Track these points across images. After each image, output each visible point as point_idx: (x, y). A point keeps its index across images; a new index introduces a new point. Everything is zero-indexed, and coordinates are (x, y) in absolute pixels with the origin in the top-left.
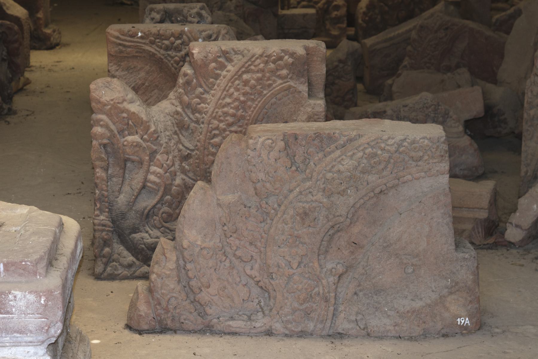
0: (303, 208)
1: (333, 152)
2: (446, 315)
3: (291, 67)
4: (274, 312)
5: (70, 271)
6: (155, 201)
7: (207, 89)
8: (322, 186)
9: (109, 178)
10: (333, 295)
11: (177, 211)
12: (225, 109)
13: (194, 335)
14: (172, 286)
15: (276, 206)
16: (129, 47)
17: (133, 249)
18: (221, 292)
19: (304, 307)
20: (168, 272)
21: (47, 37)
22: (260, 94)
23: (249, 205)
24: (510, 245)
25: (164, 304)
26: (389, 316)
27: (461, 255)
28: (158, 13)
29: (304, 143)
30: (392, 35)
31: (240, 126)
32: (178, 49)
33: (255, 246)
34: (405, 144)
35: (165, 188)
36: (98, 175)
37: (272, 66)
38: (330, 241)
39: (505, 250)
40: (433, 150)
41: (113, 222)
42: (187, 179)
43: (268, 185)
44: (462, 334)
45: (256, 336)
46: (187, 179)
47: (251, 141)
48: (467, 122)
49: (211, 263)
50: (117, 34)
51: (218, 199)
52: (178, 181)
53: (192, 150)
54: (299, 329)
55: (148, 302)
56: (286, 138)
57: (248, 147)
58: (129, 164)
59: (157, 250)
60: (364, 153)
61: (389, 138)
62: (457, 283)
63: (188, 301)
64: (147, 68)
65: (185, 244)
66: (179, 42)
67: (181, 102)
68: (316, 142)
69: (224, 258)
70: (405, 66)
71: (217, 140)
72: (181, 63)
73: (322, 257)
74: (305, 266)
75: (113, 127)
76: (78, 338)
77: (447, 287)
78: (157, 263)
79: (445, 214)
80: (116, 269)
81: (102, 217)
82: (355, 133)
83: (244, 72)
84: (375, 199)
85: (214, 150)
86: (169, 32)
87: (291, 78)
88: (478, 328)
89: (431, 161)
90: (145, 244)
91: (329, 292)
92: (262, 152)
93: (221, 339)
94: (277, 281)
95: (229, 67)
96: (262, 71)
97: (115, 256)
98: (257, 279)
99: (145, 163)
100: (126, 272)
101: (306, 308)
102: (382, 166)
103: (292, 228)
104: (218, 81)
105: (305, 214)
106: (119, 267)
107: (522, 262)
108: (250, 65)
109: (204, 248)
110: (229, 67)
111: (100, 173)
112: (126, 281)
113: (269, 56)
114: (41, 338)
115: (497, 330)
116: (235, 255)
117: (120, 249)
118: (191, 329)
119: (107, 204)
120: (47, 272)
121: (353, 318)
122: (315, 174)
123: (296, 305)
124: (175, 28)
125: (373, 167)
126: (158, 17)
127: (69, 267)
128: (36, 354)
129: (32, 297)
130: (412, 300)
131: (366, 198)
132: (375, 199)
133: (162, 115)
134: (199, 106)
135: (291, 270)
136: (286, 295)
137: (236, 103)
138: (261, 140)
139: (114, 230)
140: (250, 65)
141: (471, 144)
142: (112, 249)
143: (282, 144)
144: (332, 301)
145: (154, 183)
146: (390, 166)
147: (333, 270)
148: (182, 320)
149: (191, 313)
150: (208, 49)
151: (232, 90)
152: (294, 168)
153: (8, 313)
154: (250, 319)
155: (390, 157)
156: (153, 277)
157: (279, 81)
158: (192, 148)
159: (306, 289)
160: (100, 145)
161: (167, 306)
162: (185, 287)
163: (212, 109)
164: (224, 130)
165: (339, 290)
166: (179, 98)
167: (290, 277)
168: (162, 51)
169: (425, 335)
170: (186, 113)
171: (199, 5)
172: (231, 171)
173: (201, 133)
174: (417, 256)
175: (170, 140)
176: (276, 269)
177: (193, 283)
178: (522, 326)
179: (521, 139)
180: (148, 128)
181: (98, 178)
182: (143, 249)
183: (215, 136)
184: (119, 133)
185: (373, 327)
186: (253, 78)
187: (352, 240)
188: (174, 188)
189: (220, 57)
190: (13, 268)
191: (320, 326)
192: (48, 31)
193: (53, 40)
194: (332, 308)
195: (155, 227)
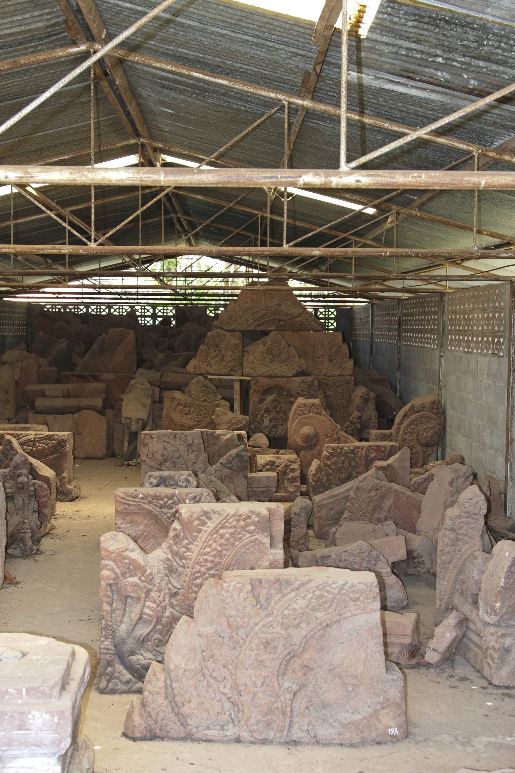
0: (266, 638)
1: (290, 593)
2: (380, 726)
3: (257, 524)
4: (242, 722)
5: (79, 694)
6: (148, 630)
7: (191, 540)
8: (281, 621)
9: (113, 611)
10: (289, 709)
11: (167, 638)
12: (206, 557)
13: (178, 742)
14: (161, 702)
15: (244, 636)
16: (132, 505)
17: (131, 668)
18: (200, 707)
19: (266, 719)
20: (158, 690)
21: (70, 492)
22: (233, 545)
23: (223, 635)
24: (428, 665)
25: (154, 716)
26: (334, 727)
27: (390, 677)
28: (155, 478)
29: (267, 586)
30: (335, 493)
31: (217, 570)
32: (170, 507)
33: (228, 668)
34: (346, 587)
35: (157, 619)
36: (104, 608)
37: (242, 523)
38: (287, 665)
39: (425, 670)
40: (368, 593)
41: (115, 646)
42: (175, 612)
43: (238, 620)
44: (392, 742)
45: (228, 743)
46: (175, 612)
47: (225, 585)
48: (393, 563)
49: (192, 682)
50: (123, 495)
51: (199, 631)
52: (167, 614)
53: (179, 589)
54: (262, 737)
55: (141, 715)
56: (252, 582)
57: (222, 589)
58: (129, 600)
59: (150, 671)
60: (314, 594)
61: (333, 583)
62: (388, 700)
63: (173, 714)
64: (146, 521)
65: (172, 667)
66: (171, 501)
67: (171, 551)
68: (276, 585)
69: (203, 678)
70: (345, 518)
71: (198, 581)
72: (172, 518)
73: (280, 678)
74: (267, 685)
75: (117, 571)
76: (84, 746)
77: (379, 703)
78: (149, 682)
79: (377, 643)
80: (116, 685)
81: (106, 643)
82: (306, 578)
83: (220, 528)
84: (322, 631)
85: (196, 589)
86: (163, 494)
87: (257, 533)
88: (405, 736)
89: (366, 601)
90: (140, 665)
91: (286, 707)
92: (234, 593)
93: (199, 745)
94: (245, 698)
95: (209, 524)
96: (235, 527)
97: (116, 674)
98: (229, 696)
99: (142, 599)
100: (124, 688)
101: (268, 720)
102: (327, 605)
103: (257, 654)
104: (200, 535)
105: (267, 644)
106: (119, 683)
107: (439, 679)
108: (225, 523)
109: (187, 670)
110: (209, 524)
111: (106, 607)
112: (124, 695)
113: (240, 516)
114: (53, 750)
115: (420, 739)
116: (211, 676)
117: (119, 667)
118: (175, 736)
119: (111, 632)
120: (60, 695)
121: (305, 728)
122: (275, 611)
123: (260, 717)
124: (168, 491)
125: (320, 606)
126: (155, 482)
127: (79, 690)
128: (49, 763)
129: (47, 717)
130: (352, 713)
131: (315, 631)
132: (322, 631)
133: (156, 561)
134: (185, 554)
135: (255, 689)
136: (251, 709)
137: (214, 552)
138: (233, 584)
139: (116, 653)
140: (225, 523)
141: (397, 582)
142: (114, 668)
143: (249, 587)
144: (289, 714)
145: (149, 615)
146: (334, 605)
147: (290, 689)
148: (168, 730)
149: (175, 723)
150: (193, 510)
151: (211, 542)
152: (259, 606)
153: (27, 729)
154: (222, 728)
155: (334, 598)
156: (146, 693)
157: (248, 535)
158: (179, 587)
159: (268, 704)
160: (107, 585)
161: (156, 718)
162: (171, 702)
163: (195, 557)
164: (205, 573)
165: (294, 705)
166: (170, 548)
167: (255, 694)
168: (158, 509)
169: (363, 743)
170: (175, 560)
171: (187, 473)
172: (209, 608)
173: (186, 576)
174: (356, 677)
175: (162, 580)
176: (244, 688)
177: (178, 699)
178: (440, 735)
179: (436, 576)
180: (145, 571)
181: (104, 611)
182: (138, 668)
183: (197, 578)
184: (122, 575)
185: (321, 736)
186: (227, 533)
187: (304, 664)
188: (164, 619)
189: (202, 516)
190: (33, 692)
191: (278, 735)
192: (70, 487)
193: (74, 494)
194: (288, 720)
195: (148, 650)
